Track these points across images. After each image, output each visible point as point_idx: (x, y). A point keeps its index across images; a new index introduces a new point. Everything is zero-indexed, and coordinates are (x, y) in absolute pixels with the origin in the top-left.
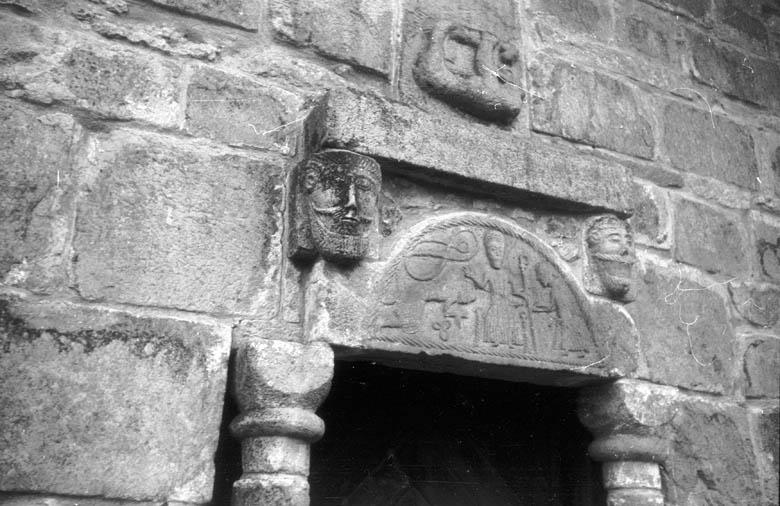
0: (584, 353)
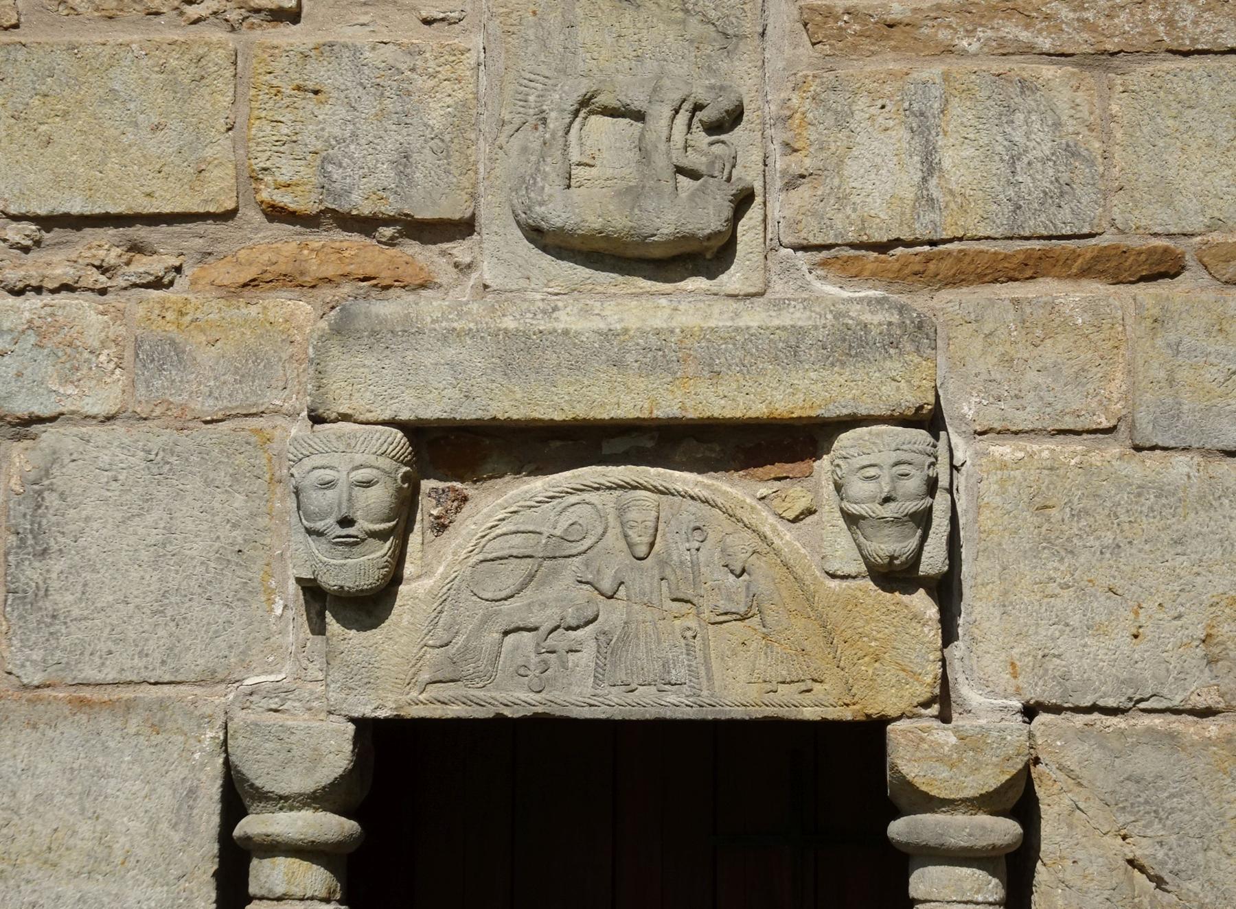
0: (810, 684)
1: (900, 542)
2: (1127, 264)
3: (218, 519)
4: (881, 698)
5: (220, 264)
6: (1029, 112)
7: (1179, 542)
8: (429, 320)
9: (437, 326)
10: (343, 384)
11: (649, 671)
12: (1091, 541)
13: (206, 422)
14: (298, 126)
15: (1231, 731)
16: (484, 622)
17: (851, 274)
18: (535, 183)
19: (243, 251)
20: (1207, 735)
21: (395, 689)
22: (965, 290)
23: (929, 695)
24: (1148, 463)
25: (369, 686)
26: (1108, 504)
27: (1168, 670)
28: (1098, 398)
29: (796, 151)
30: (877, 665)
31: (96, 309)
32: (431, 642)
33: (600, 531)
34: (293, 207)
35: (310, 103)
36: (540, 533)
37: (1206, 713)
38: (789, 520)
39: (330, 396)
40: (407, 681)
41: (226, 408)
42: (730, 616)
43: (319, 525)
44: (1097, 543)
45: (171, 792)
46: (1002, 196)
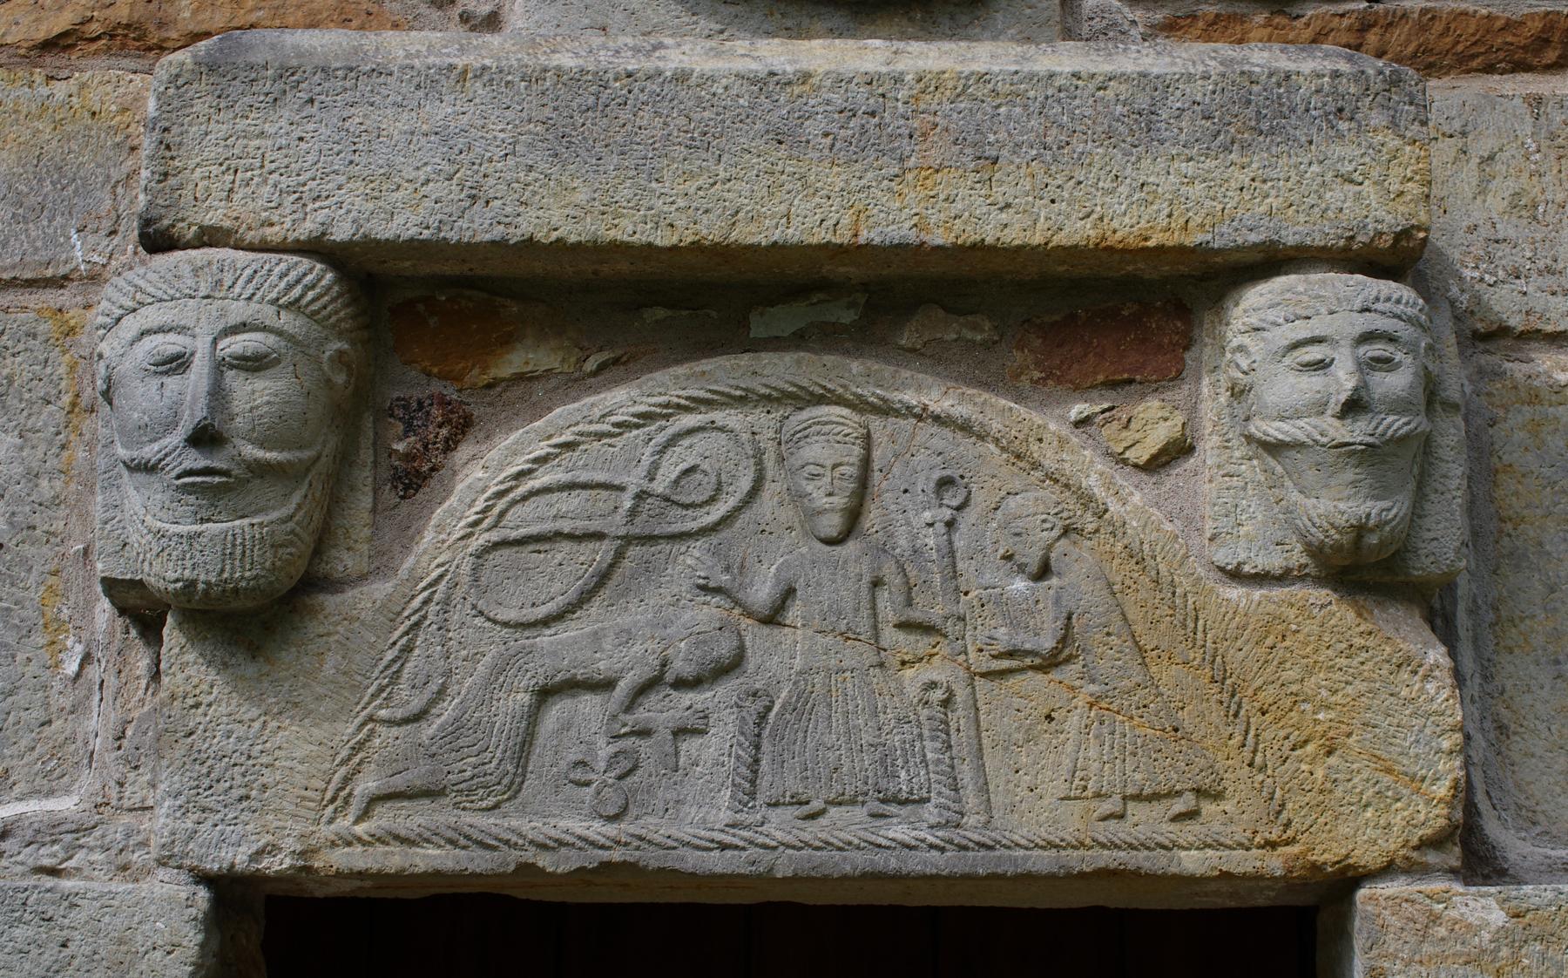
1: (1377, 498)
4: (1344, 830)
8: (401, 53)
10: (215, 170)
16: (499, 669)
21: (303, 812)
23: (1442, 822)
25: (245, 804)
30: (1332, 760)
32: (383, 713)
33: (745, 484)
36: (621, 488)
38: (1136, 466)
39: (187, 193)
40: (329, 795)
43: (150, 452)
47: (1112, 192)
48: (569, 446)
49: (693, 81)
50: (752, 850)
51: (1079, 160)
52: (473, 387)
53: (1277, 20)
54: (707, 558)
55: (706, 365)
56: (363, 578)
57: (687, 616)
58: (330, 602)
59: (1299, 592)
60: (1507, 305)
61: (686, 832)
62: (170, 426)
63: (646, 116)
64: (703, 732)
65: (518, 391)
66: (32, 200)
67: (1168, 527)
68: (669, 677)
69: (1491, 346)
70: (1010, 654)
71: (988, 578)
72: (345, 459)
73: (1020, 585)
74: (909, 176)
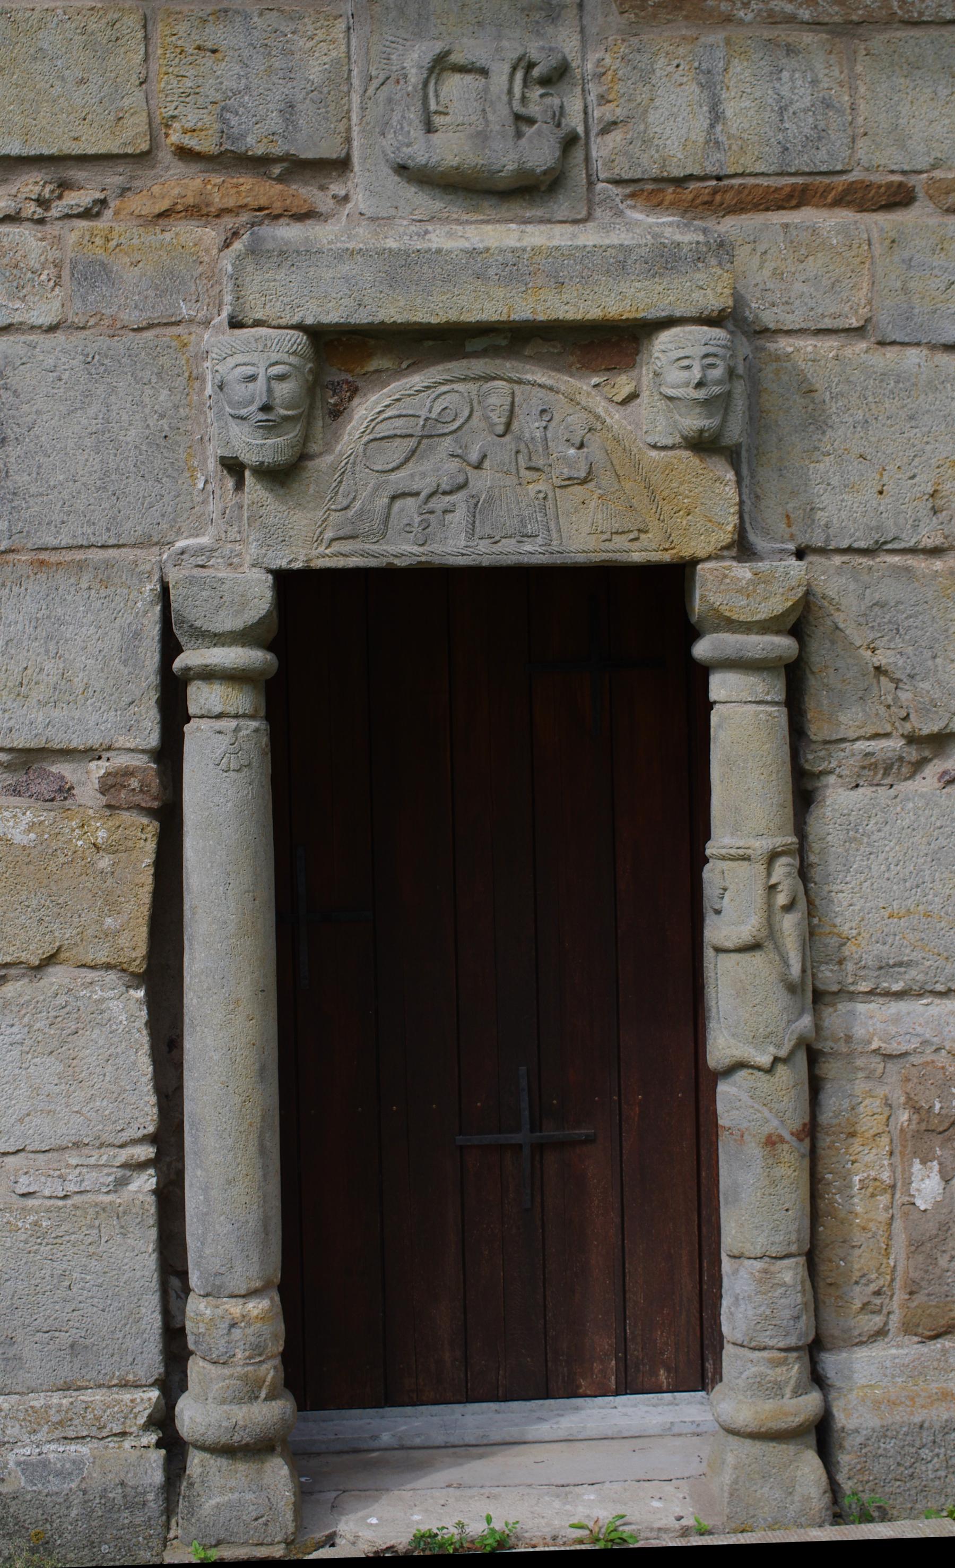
1: (708, 419)
2: (871, 195)
3: (147, 410)
5: (137, 197)
6: (793, 71)
7: (911, 418)
8: (325, 241)
9: (333, 246)
11: (510, 526)
12: (846, 418)
13: (134, 330)
14: (201, 81)
15: (952, 565)
16: (376, 489)
17: (655, 203)
18: (402, 128)
19: (155, 187)
20: (935, 568)
22: (743, 216)
23: (730, 540)
24: (888, 355)
26: (859, 389)
27: (906, 519)
28: (850, 303)
29: (610, 102)
30: (689, 517)
31: (35, 236)
32: (333, 507)
33: (466, 413)
34: (198, 148)
35: (208, 61)
36: (419, 417)
37: (935, 552)
41: (150, 318)
42: (571, 481)
43: (243, 412)
44: (851, 419)
45: (119, 634)
46: (773, 140)
47: (607, 296)
48: (398, 400)
49: (443, 253)
50: (474, 556)
51: (596, 283)
52: (358, 375)
53: (679, 190)
54: (454, 444)
55: (450, 365)
56: (321, 454)
57: (446, 466)
58: (310, 464)
59: (678, 452)
60: (769, 318)
61: (449, 550)
62: (251, 402)
63: (425, 267)
64: (453, 511)
65: (375, 376)
66: (163, 287)
67: (629, 428)
68: (440, 491)
69: (762, 336)
70: (569, 479)
71: (560, 449)
72: (312, 407)
73: (572, 451)
74: (529, 291)
